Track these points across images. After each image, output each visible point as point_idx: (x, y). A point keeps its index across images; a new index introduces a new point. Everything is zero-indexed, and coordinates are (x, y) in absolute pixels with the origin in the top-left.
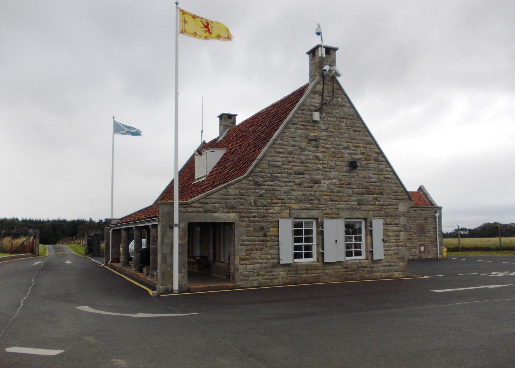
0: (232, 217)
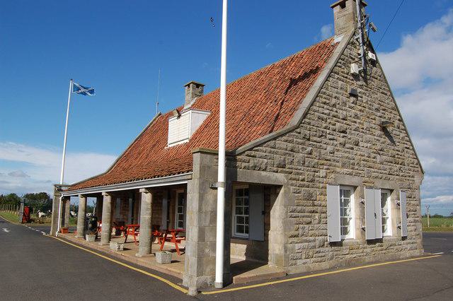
0: (280, 178)
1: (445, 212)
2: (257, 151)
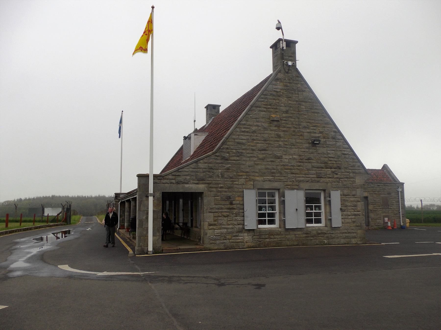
0: (201, 187)
1: (440, 205)
2: (180, 172)
